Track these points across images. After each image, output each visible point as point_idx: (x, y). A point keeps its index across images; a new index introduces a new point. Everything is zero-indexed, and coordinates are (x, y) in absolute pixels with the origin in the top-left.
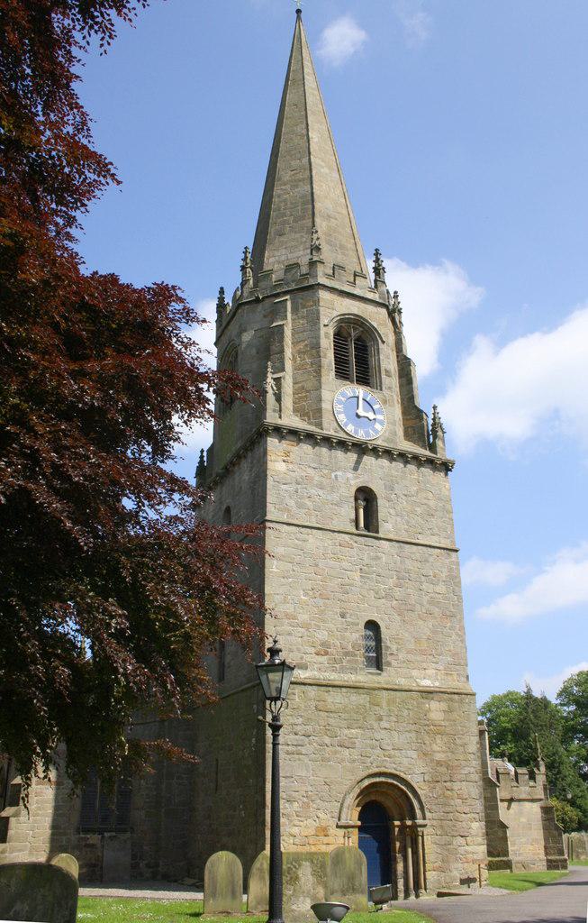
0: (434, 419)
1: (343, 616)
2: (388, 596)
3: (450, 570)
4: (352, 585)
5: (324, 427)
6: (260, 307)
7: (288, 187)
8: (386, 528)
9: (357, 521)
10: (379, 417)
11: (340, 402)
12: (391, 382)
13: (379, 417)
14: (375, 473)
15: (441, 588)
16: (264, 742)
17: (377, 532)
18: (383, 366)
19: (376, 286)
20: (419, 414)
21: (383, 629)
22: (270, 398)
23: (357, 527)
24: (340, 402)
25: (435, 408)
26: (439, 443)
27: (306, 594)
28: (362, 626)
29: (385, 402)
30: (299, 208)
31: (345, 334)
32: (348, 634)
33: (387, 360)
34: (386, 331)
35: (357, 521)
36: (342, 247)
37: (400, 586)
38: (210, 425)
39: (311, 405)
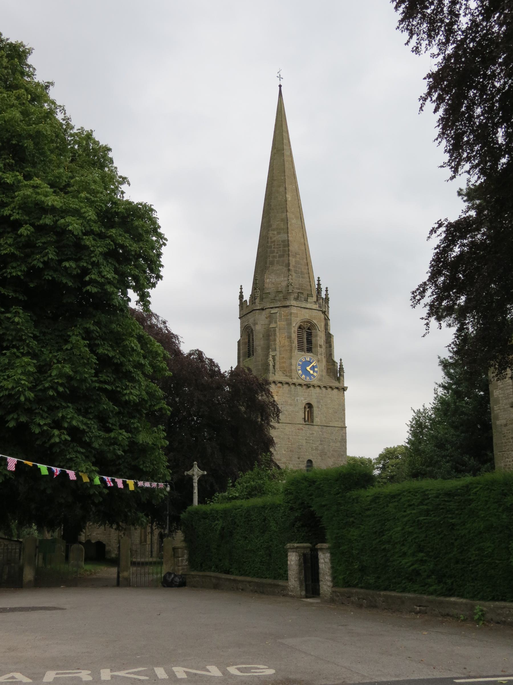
0: (340, 366)
1: (299, 458)
2: (316, 449)
3: (342, 436)
4: (302, 446)
5: (293, 377)
6: (264, 312)
7: (275, 232)
8: (317, 420)
9: (305, 418)
10: (315, 374)
11: (299, 365)
12: (322, 351)
13: (315, 374)
14: (313, 396)
15: (338, 444)
16: (196, 670)
17: (313, 422)
18: (319, 343)
19: (317, 300)
20: (334, 363)
21: (314, 463)
22: (271, 367)
23: (305, 422)
24: (299, 365)
25: (341, 360)
26: (342, 378)
27: (285, 451)
28: (305, 462)
29: (318, 361)
30: (281, 249)
31: (302, 327)
32: (300, 465)
33: (320, 339)
34: (321, 326)
35: (305, 418)
36: (302, 273)
37: (321, 444)
38: (328, 555)
39: (288, 371)
